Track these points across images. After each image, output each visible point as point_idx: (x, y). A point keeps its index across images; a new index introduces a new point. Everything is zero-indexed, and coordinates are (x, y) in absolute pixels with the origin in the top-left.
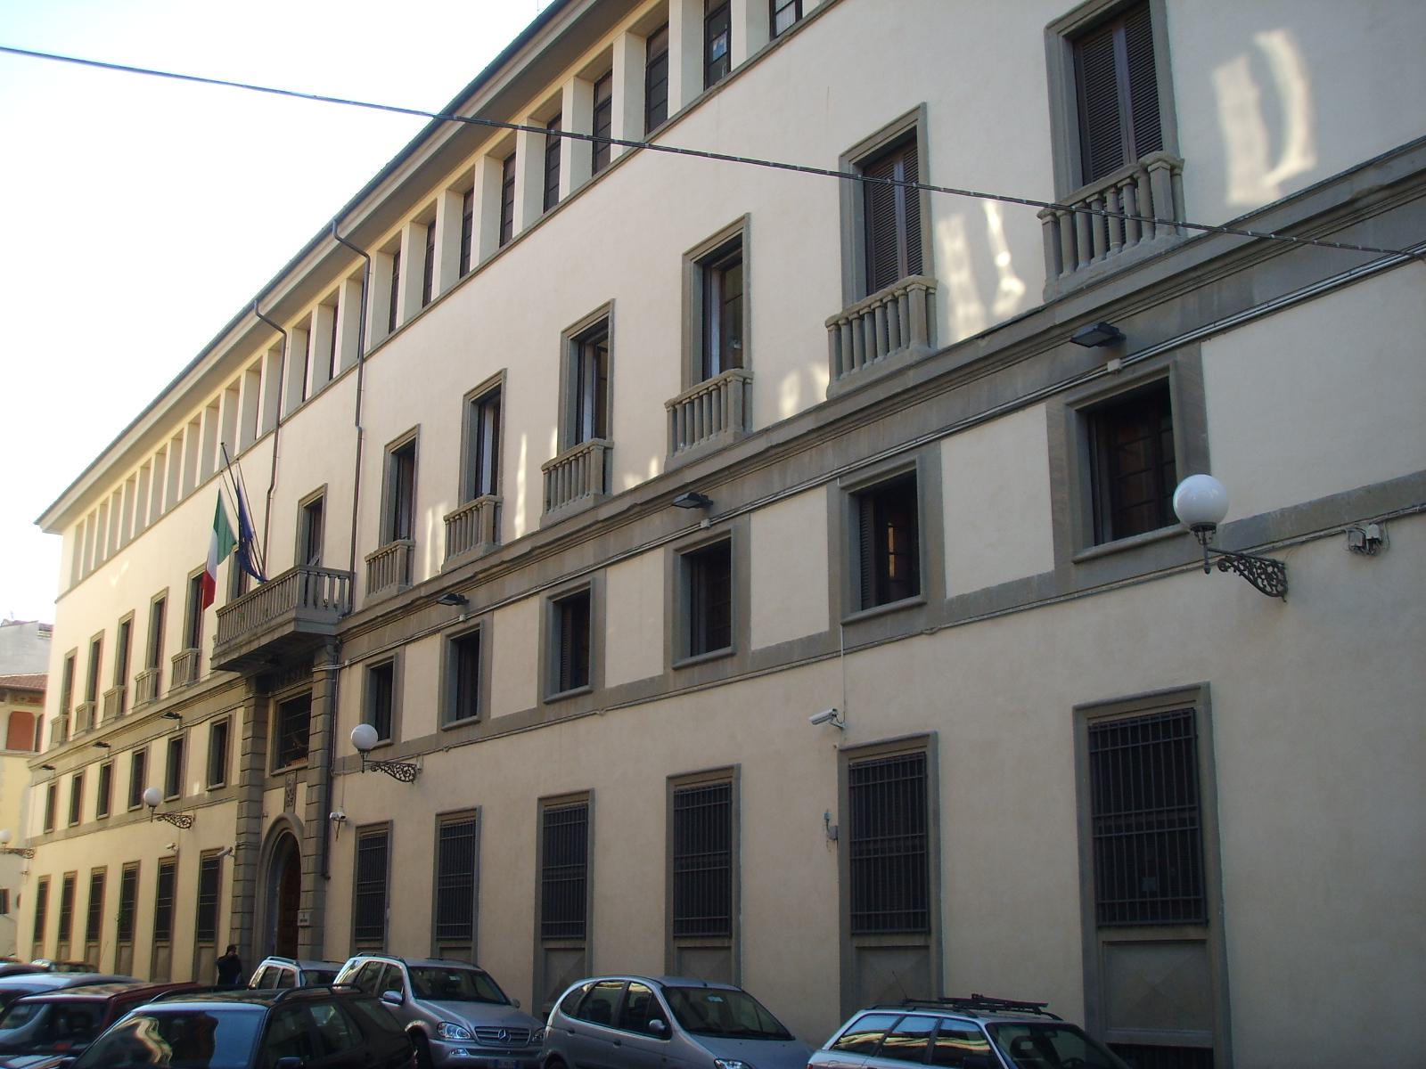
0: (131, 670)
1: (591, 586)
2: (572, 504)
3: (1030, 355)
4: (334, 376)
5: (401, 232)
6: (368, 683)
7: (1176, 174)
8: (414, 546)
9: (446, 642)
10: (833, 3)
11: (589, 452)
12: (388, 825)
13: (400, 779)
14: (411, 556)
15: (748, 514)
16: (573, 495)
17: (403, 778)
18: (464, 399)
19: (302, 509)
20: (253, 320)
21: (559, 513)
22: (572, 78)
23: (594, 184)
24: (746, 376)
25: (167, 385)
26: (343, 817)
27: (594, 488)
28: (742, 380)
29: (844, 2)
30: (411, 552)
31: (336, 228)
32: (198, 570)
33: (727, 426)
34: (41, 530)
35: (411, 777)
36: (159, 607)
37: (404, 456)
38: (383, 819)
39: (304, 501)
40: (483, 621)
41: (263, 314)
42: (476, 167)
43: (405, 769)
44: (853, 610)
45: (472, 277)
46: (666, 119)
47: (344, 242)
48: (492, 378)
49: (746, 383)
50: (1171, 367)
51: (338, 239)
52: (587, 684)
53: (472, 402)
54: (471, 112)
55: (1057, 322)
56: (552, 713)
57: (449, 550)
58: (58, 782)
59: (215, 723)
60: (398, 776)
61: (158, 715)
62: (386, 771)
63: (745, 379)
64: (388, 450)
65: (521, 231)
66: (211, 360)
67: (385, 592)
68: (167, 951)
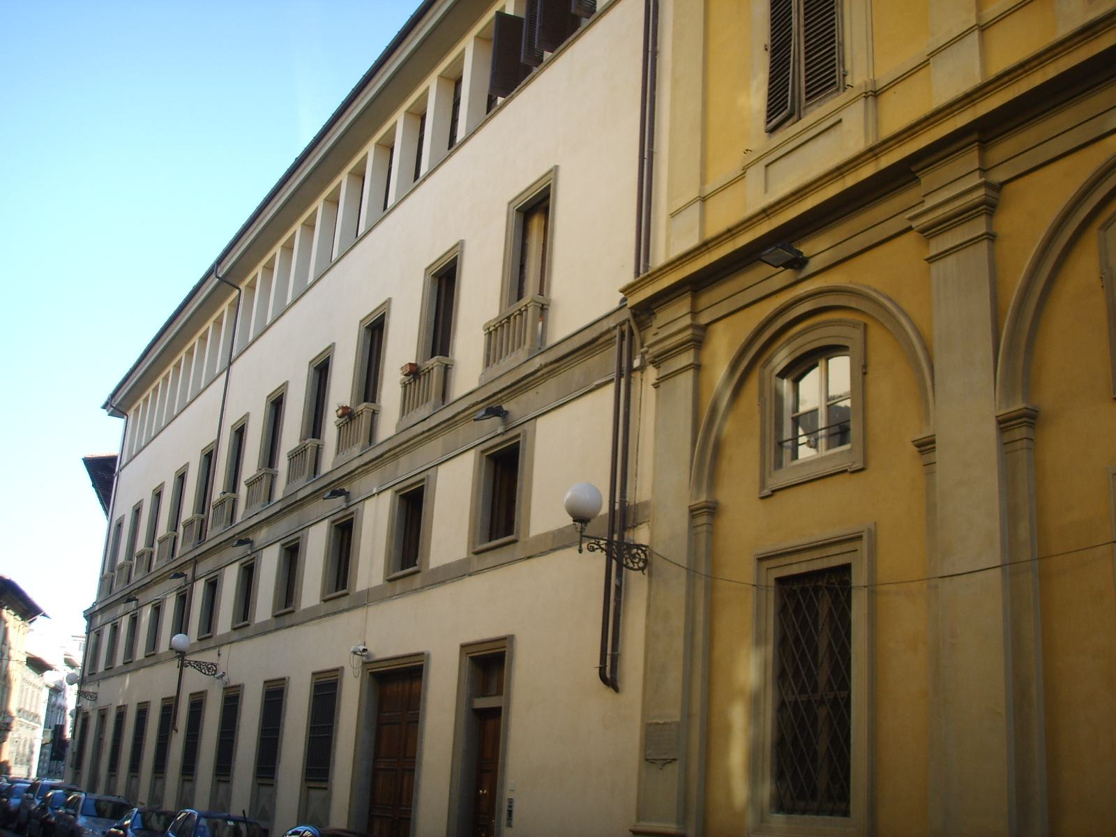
0: (182, 518)
1: (521, 439)
2: (496, 366)
3: (567, 369)
4: (388, 207)
5: (464, 50)
6: (282, 561)
7: (545, 309)
8: (323, 445)
9: (331, 526)
10: (614, 2)
11: (362, 413)
12: (338, 673)
13: (205, 673)
14: (449, 374)
15: (533, 420)
16: (515, 348)
17: (207, 673)
18: (425, 273)
19: (429, 278)
20: (214, 281)
21: (496, 370)
22: (473, 38)
23: (450, 156)
24: (375, 409)
25: (157, 332)
26: (365, 650)
27: (363, 440)
28: (541, 306)
29: (621, 2)
30: (376, 415)
31: (217, 267)
32: (238, 424)
33: (524, 343)
34: (107, 413)
35: (213, 672)
36: (181, 478)
37: (240, 433)
38: (502, 634)
39: (365, 322)
40: (428, 476)
41: (220, 276)
42: (398, 122)
43: (209, 666)
44: (481, 543)
45: (424, 180)
46: (595, 11)
47: (222, 280)
48: (276, 390)
49: (374, 413)
50: (522, 435)
51: (217, 277)
52: (416, 565)
53: (433, 276)
54: (221, 272)
55: (298, 499)
56: (477, 563)
57: (338, 449)
58: (222, 575)
59: (209, 579)
60: (203, 671)
61: (315, 495)
62: (195, 667)
63: (318, 445)
64: (362, 324)
65: (427, 170)
66: (174, 328)
67: (301, 482)
68: (323, 793)
